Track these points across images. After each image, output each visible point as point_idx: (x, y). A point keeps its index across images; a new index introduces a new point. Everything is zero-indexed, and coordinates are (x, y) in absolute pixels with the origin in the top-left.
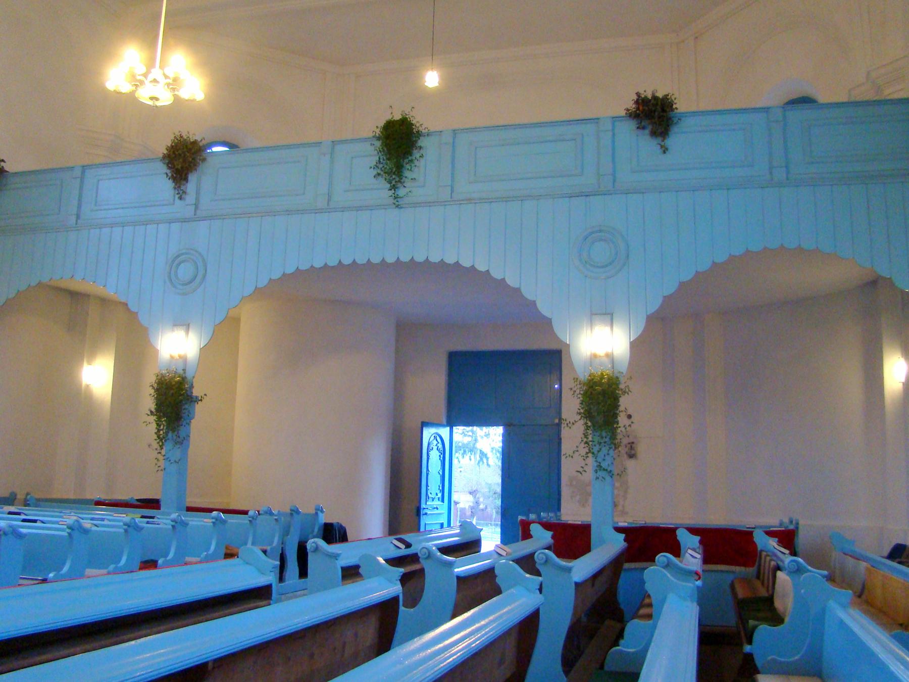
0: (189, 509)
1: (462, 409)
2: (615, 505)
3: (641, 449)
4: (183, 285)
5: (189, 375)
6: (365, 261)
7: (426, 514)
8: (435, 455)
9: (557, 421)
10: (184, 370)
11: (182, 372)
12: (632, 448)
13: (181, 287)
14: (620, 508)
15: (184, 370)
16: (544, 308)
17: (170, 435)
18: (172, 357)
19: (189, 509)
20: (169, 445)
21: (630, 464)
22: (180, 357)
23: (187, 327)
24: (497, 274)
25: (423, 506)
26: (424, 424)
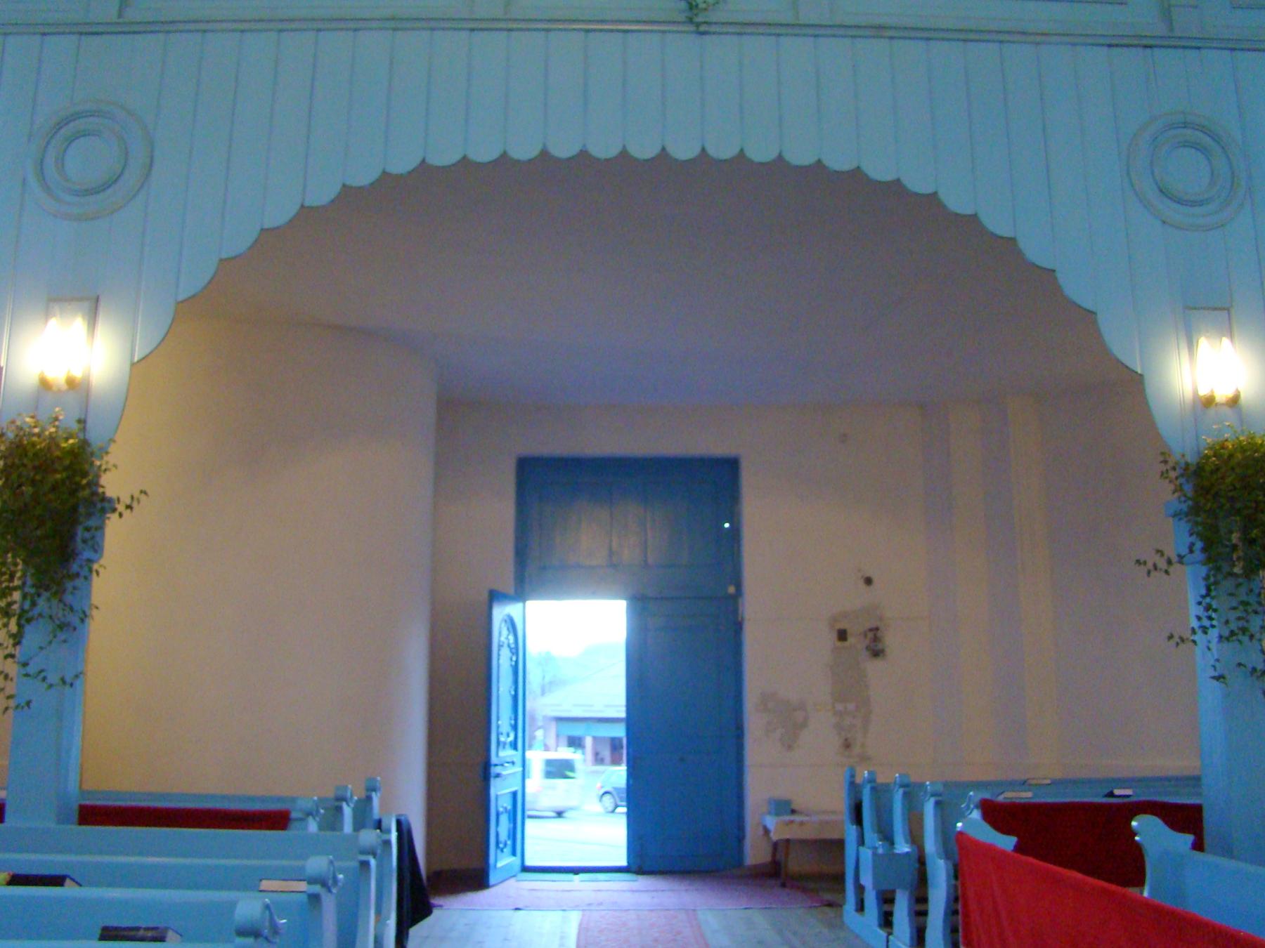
0: (92, 815)
1: (532, 571)
2: (847, 745)
3: (891, 640)
4: (78, 194)
5: (95, 436)
6: (612, 152)
7: (498, 775)
8: (505, 653)
9: (732, 590)
10: (82, 422)
11: (75, 427)
12: (876, 639)
13: (68, 198)
14: (857, 749)
15: (82, 422)
16: (1076, 288)
17: (42, 603)
18: (45, 385)
19: (92, 815)
20: (34, 636)
21: (874, 668)
22: (71, 383)
23: (93, 308)
24: (957, 202)
25: (494, 760)
26: (495, 596)
